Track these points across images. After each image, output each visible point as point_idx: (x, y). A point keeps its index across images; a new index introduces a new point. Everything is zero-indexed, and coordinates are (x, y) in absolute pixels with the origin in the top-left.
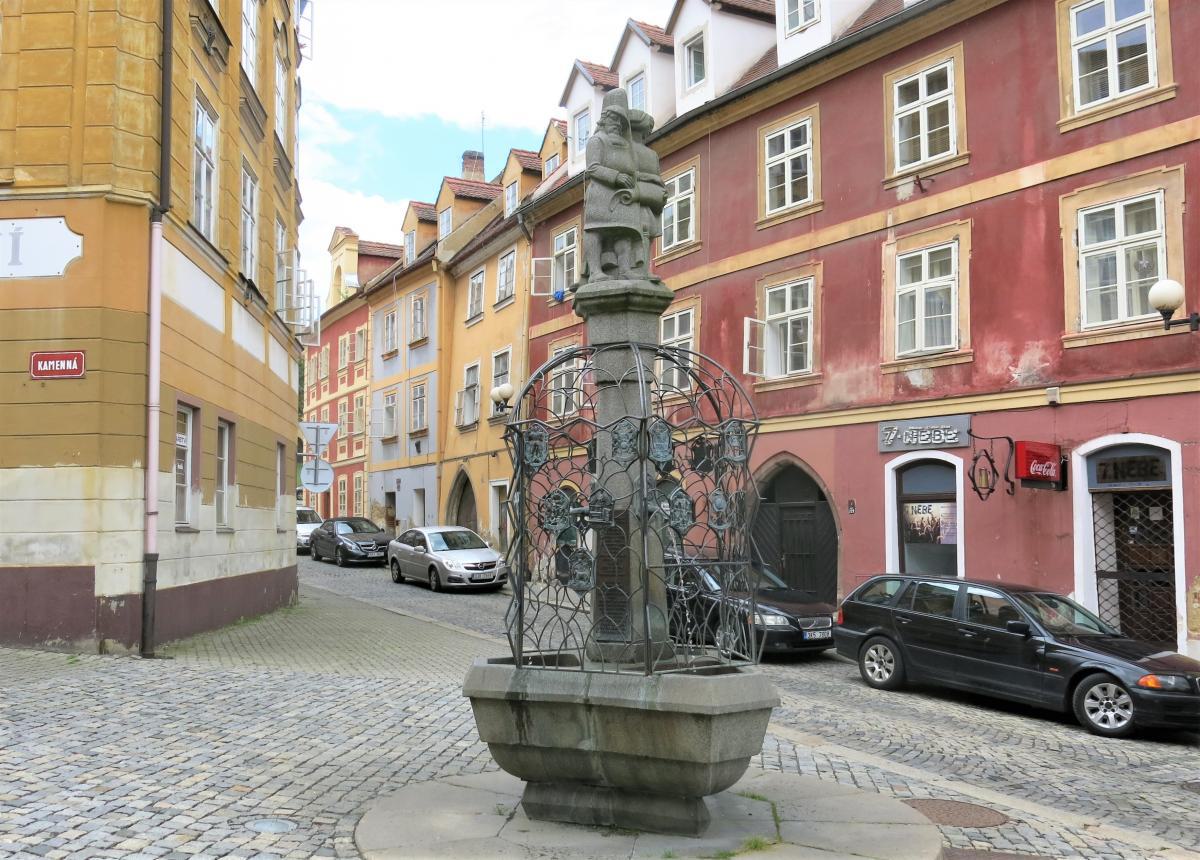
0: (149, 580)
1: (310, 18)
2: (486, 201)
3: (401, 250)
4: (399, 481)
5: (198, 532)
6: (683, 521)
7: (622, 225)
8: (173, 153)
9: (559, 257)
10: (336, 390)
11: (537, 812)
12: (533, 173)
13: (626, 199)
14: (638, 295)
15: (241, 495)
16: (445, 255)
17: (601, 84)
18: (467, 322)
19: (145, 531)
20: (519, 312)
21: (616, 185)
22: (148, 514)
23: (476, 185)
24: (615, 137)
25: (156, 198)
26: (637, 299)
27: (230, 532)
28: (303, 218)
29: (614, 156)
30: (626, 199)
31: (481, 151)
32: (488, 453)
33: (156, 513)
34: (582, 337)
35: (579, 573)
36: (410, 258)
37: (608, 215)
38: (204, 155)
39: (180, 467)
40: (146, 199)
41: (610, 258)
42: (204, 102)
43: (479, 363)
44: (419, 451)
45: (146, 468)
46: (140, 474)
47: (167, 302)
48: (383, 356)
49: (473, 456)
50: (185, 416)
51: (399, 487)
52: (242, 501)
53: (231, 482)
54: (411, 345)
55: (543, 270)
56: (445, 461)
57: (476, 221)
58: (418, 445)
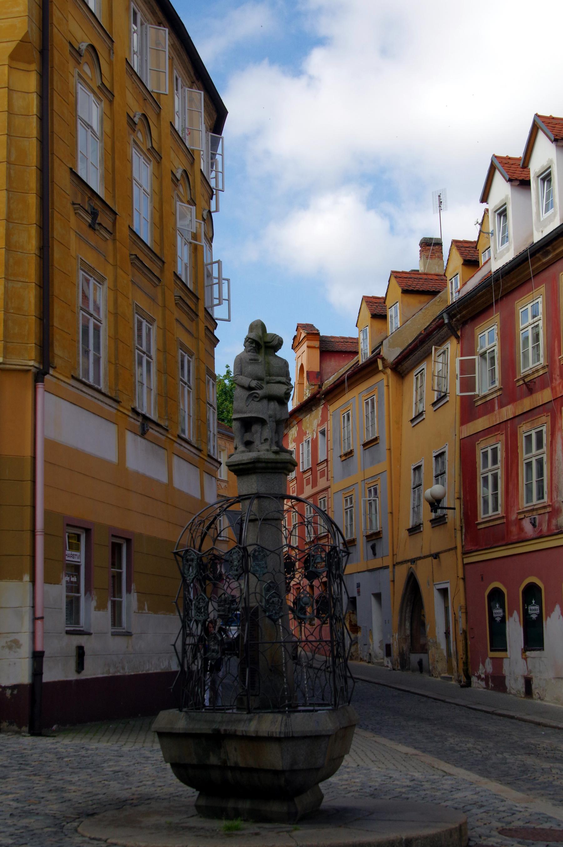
0: (37, 673)
1: (221, 153)
2: (434, 293)
3: (355, 342)
4: (358, 585)
5: (90, 634)
6: (276, 613)
7: (253, 415)
8: (56, 323)
9: (483, 355)
10: (316, 485)
11: (204, 812)
12: (472, 263)
13: (256, 397)
14: (262, 462)
15: (139, 601)
16: (391, 353)
17: (516, 180)
18: (412, 421)
19: (34, 633)
20: (452, 410)
21: (250, 388)
22: (35, 619)
23: (425, 277)
24: (251, 355)
25: (40, 363)
26: (260, 465)
27: (128, 634)
28: (218, 341)
30: (256, 397)
31: (438, 236)
32: (431, 555)
33: (42, 618)
34: (504, 436)
35: (213, 648)
36: (365, 350)
38: (91, 315)
39: (74, 579)
40: (31, 366)
41: (248, 437)
42: (89, 270)
43: (423, 463)
44: (375, 554)
45: (33, 581)
46: (29, 586)
47: (50, 444)
48: (341, 457)
49: (420, 558)
50: (78, 537)
51: (359, 592)
52: (141, 608)
53: (129, 591)
54: (364, 445)
55: (467, 368)
56: (398, 563)
57: (428, 312)
58: (373, 548)
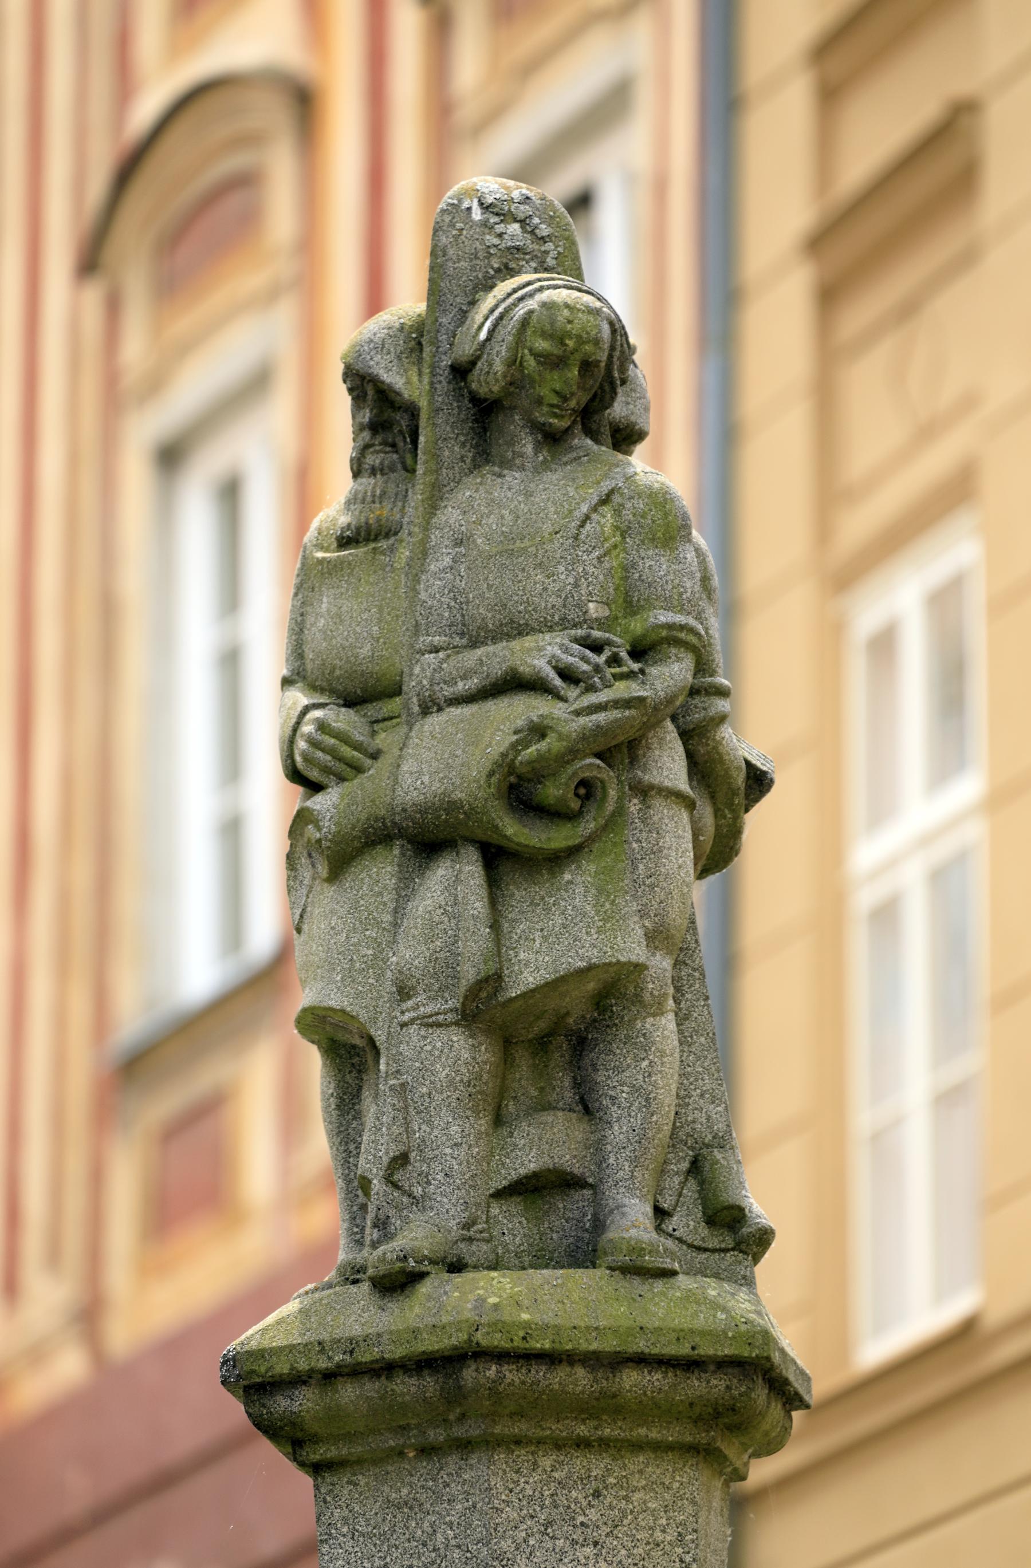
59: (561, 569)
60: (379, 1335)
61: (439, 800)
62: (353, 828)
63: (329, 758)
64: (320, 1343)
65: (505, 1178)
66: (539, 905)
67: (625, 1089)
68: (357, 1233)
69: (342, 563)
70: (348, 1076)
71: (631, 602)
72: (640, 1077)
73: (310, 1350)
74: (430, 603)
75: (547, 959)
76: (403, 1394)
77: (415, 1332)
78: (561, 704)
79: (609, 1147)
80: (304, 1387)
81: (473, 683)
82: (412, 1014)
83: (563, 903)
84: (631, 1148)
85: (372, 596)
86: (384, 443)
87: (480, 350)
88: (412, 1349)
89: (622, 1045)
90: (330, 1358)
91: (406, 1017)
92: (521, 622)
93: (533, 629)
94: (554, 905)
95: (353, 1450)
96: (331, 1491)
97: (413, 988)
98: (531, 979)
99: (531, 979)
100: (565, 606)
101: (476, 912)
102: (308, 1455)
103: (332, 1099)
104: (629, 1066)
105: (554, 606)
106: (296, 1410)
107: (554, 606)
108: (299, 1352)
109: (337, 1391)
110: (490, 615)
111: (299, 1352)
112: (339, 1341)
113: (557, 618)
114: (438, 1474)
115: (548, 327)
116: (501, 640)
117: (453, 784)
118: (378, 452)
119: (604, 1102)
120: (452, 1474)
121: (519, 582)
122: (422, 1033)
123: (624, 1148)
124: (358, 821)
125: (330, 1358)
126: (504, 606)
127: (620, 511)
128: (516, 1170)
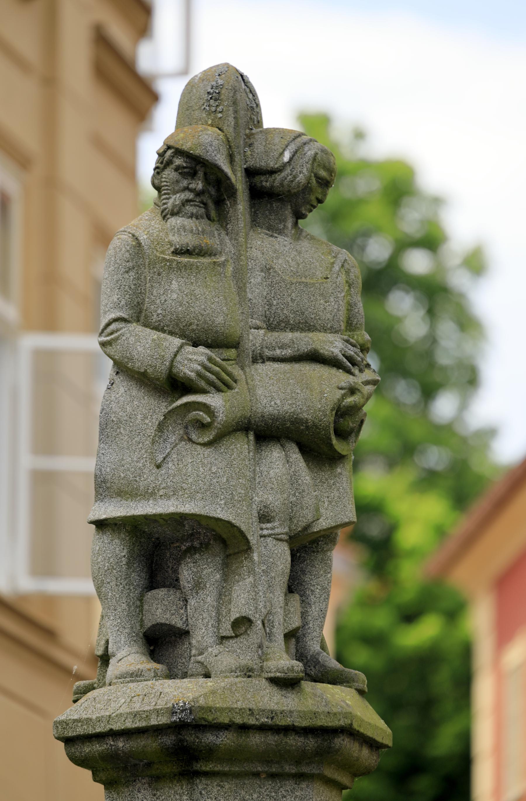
21: (175, 385)
29: (173, 294)
30: (203, 426)
37: (150, 478)
41: (161, 608)
59: (332, 299)
60: (291, 712)
61: (289, 416)
62: (233, 420)
63: (214, 377)
64: (250, 710)
65: (286, 628)
66: (325, 483)
67: (319, 587)
68: (134, 636)
69: (192, 265)
70: (136, 548)
71: (351, 324)
72: (326, 582)
73: (243, 713)
74: (254, 301)
75: (331, 514)
76: (292, 746)
77: (315, 714)
78: (351, 377)
79: (310, 618)
80: (226, 731)
81: (288, 352)
82: (270, 532)
83: (338, 485)
84: (320, 620)
85: (218, 289)
86: (202, 202)
87: (283, 167)
88: (314, 723)
89: (319, 563)
90: (257, 719)
91: (265, 532)
92: (311, 324)
93: (317, 329)
94: (333, 484)
95: (233, 769)
96: (205, 788)
97: (273, 517)
98: (324, 524)
99: (324, 524)
100: (333, 320)
101: (307, 482)
102: (201, 766)
103: (123, 559)
104: (322, 575)
105: (329, 319)
106: (218, 743)
107: (329, 319)
108: (236, 713)
109: (248, 737)
110: (292, 316)
111: (236, 713)
112: (264, 711)
113: (329, 326)
114: (279, 790)
115: (327, 164)
116: (297, 330)
117: (301, 409)
118: (195, 205)
119: (307, 593)
120: (288, 791)
121: (312, 301)
122: (274, 543)
123: (317, 619)
124: (236, 417)
125: (257, 719)
126: (303, 313)
127: (349, 273)
128: (291, 624)
